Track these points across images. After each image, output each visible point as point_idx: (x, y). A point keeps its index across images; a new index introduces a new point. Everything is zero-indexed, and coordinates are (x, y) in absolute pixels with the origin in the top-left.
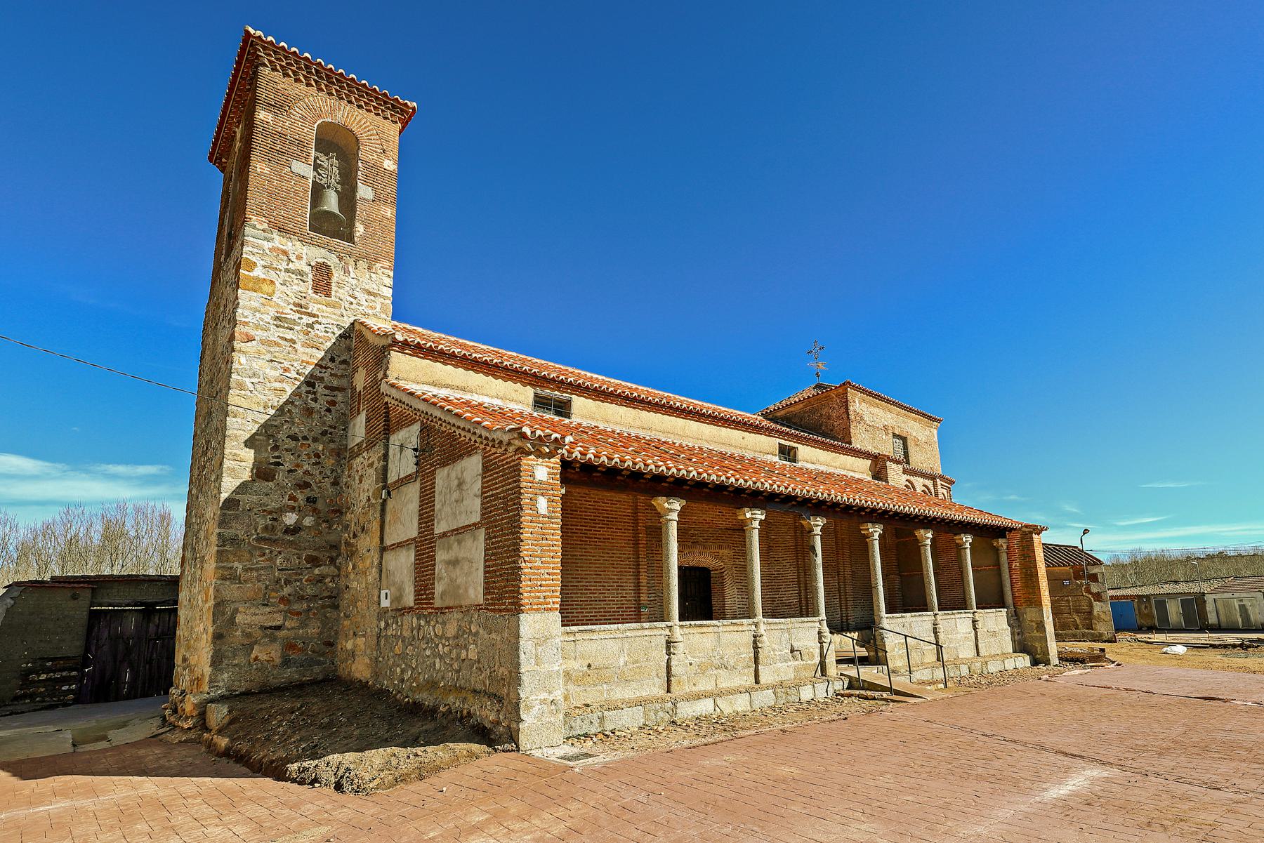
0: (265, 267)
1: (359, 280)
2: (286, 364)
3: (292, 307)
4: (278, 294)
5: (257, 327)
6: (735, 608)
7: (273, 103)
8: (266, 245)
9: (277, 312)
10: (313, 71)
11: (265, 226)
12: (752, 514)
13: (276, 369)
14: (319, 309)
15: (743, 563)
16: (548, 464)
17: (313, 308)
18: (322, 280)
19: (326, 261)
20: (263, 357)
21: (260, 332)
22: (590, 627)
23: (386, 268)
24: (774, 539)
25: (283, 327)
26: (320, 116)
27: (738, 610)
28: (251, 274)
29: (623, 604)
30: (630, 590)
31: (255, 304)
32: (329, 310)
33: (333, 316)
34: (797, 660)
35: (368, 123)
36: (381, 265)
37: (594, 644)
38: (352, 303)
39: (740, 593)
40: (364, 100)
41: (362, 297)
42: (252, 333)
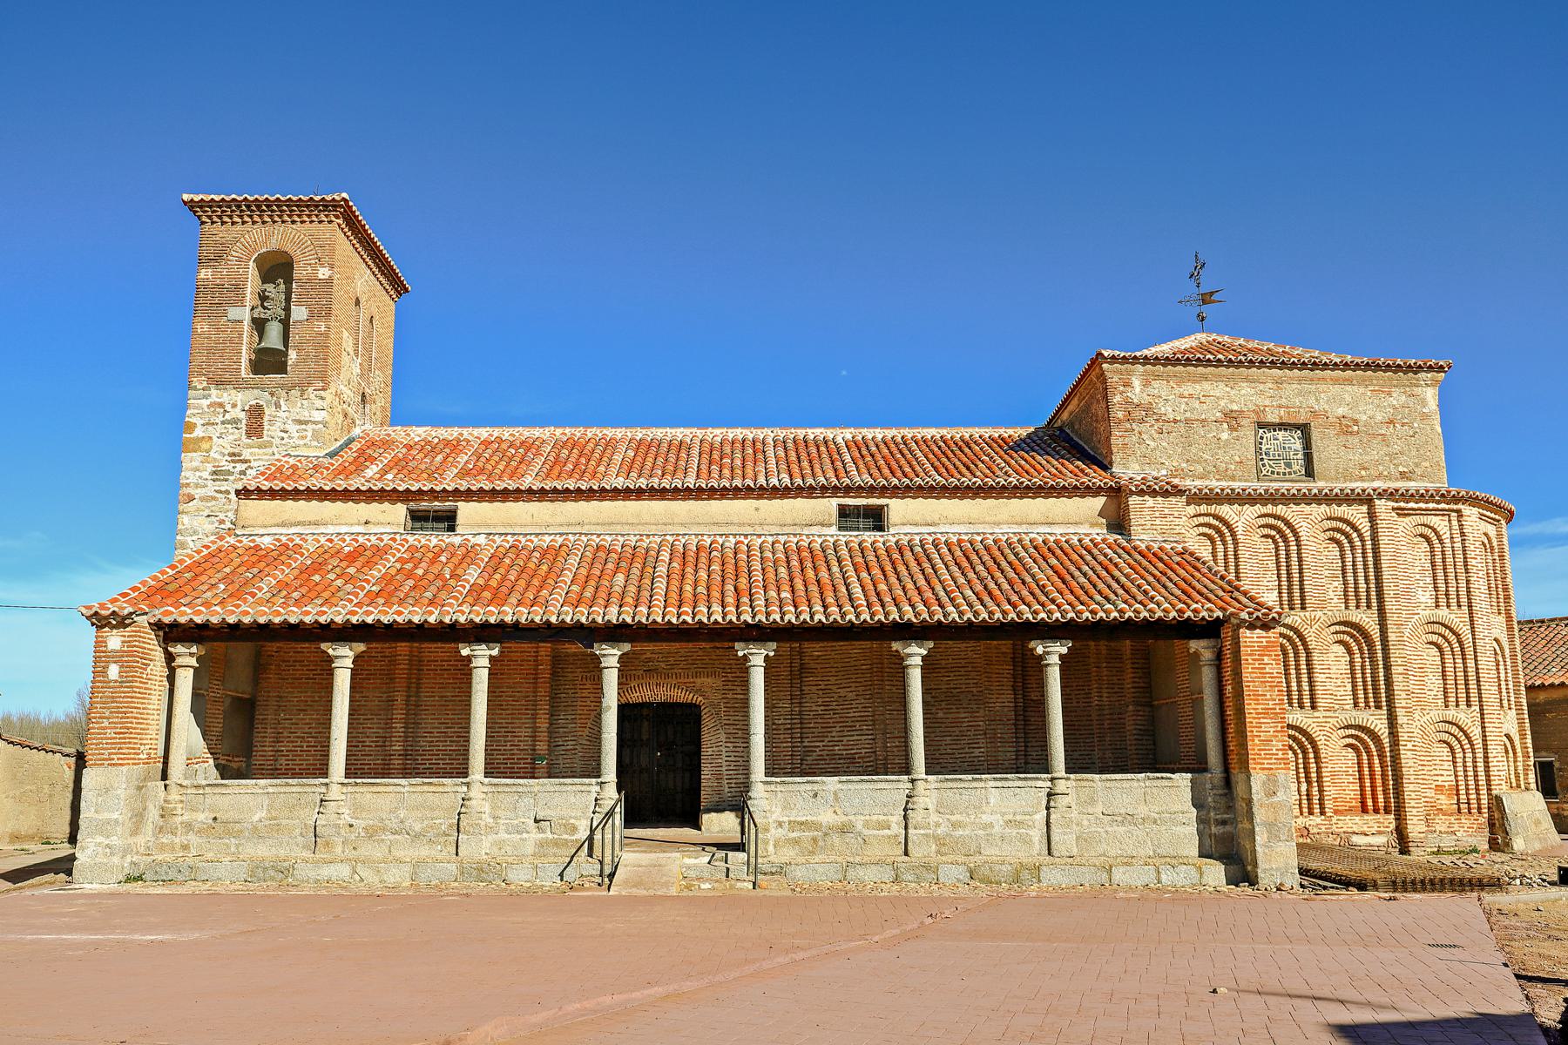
0: (203, 425)
1: (290, 412)
2: (222, 516)
3: (227, 458)
4: (215, 448)
5: (197, 486)
6: (720, 761)
7: (213, 257)
8: (205, 402)
9: (214, 467)
10: (244, 207)
11: (205, 384)
12: (471, 650)
13: (213, 523)
14: (251, 454)
15: (742, 697)
16: (124, 634)
17: (246, 454)
18: (255, 422)
19: (258, 401)
20: (201, 513)
21: (199, 490)
22: (1005, 776)
23: (319, 390)
24: (819, 656)
25: (220, 480)
26: (255, 250)
27: (724, 764)
28: (192, 436)
29: (513, 754)
30: (525, 736)
31: (195, 464)
32: (261, 451)
33: (265, 457)
34: (543, 832)
35: (302, 236)
36: (313, 388)
37: (226, 799)
38: (283, 439)
39: (732, 740)
40: (296, 213)
41: (293, 428)
42: (193, 492)
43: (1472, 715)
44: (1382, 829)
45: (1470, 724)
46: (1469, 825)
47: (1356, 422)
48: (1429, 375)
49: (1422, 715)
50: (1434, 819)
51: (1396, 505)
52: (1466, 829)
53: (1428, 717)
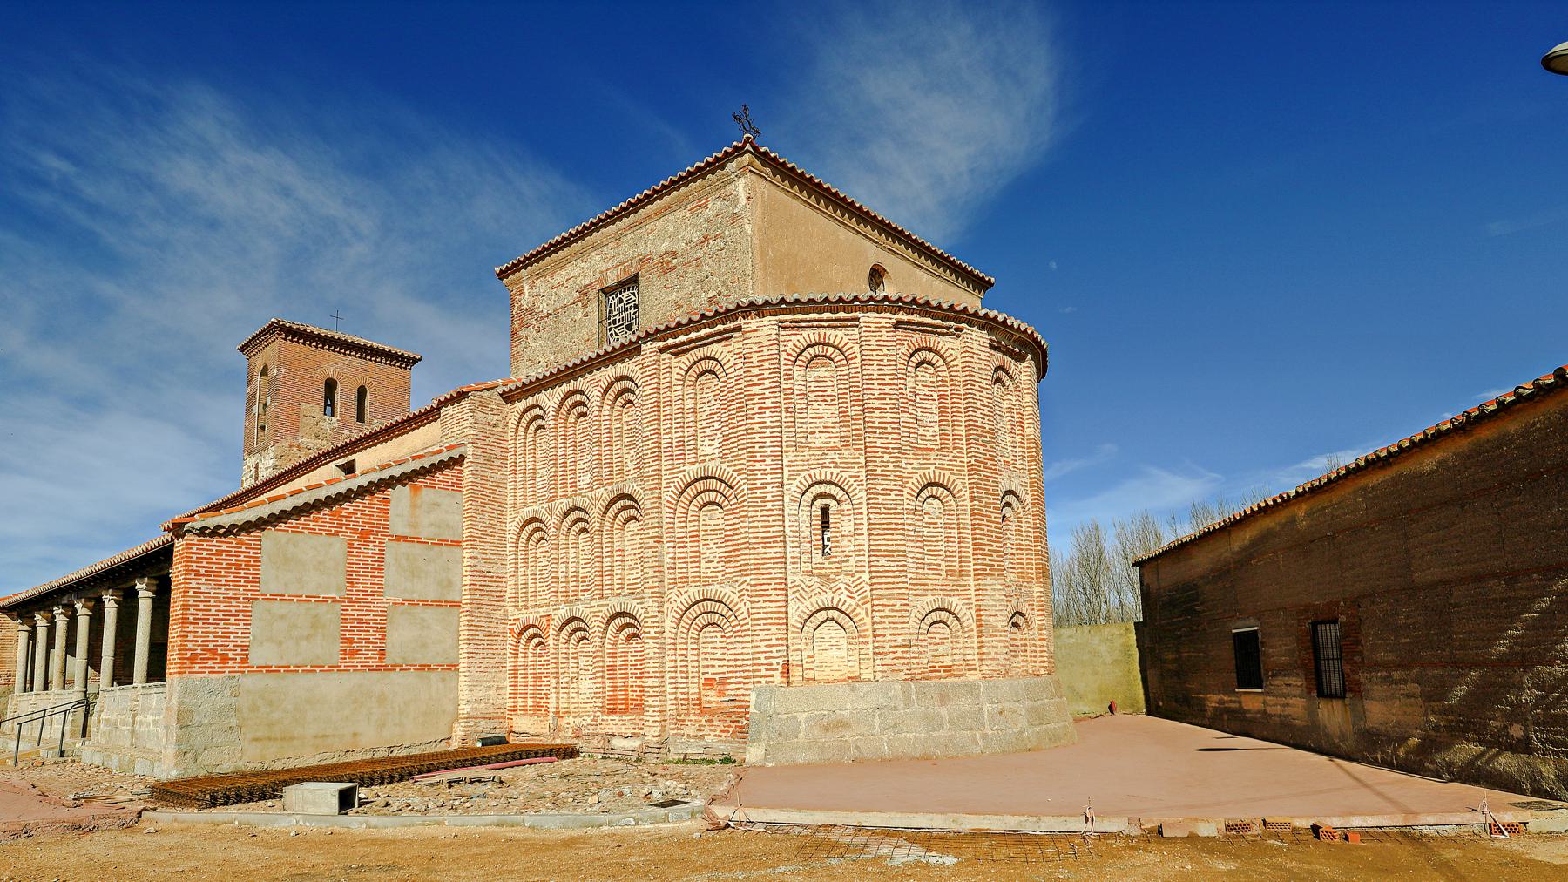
43: (741, 588)
44: (637, 731)
45: (736, 600)
46: (723, 729)
47: (674, 254)
48: (734, 164)
49: (678, 593)
50: (684, 721)
51: (661, 344)
52: (717, 733)
53: (686, 596)
